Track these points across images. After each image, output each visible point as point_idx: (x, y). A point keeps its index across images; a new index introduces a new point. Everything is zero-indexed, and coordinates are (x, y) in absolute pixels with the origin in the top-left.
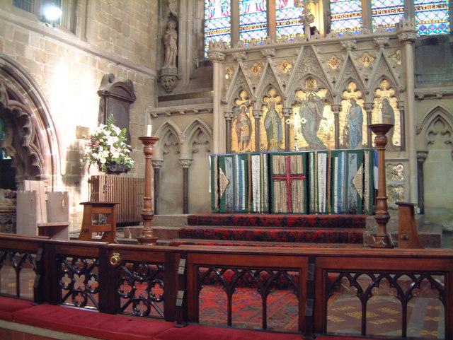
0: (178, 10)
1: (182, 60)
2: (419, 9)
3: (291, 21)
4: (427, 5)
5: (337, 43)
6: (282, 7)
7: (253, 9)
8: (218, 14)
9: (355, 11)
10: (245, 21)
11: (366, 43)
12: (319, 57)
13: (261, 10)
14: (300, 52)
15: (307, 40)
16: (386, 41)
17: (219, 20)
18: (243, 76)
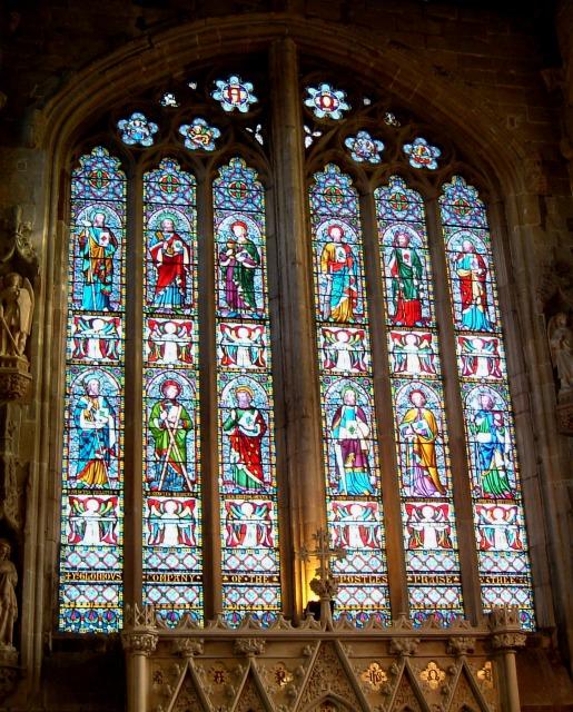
0: (22, 515)
1: (28, 631)
2: (485, 581)
3: (251, 575)
4: (498, 575)
5: (230, 642)
6: (233, 544)
7: (171, 538)
8: (92, 536)
9: (376, 572)
10: (155, 562)
11: (433, 645)
12: (350, 663)
13: (188, 543)
14: (314, 652)
15: (327, 630)
16: (471, 644)
17: (96, 550)
18: (259, 692)
